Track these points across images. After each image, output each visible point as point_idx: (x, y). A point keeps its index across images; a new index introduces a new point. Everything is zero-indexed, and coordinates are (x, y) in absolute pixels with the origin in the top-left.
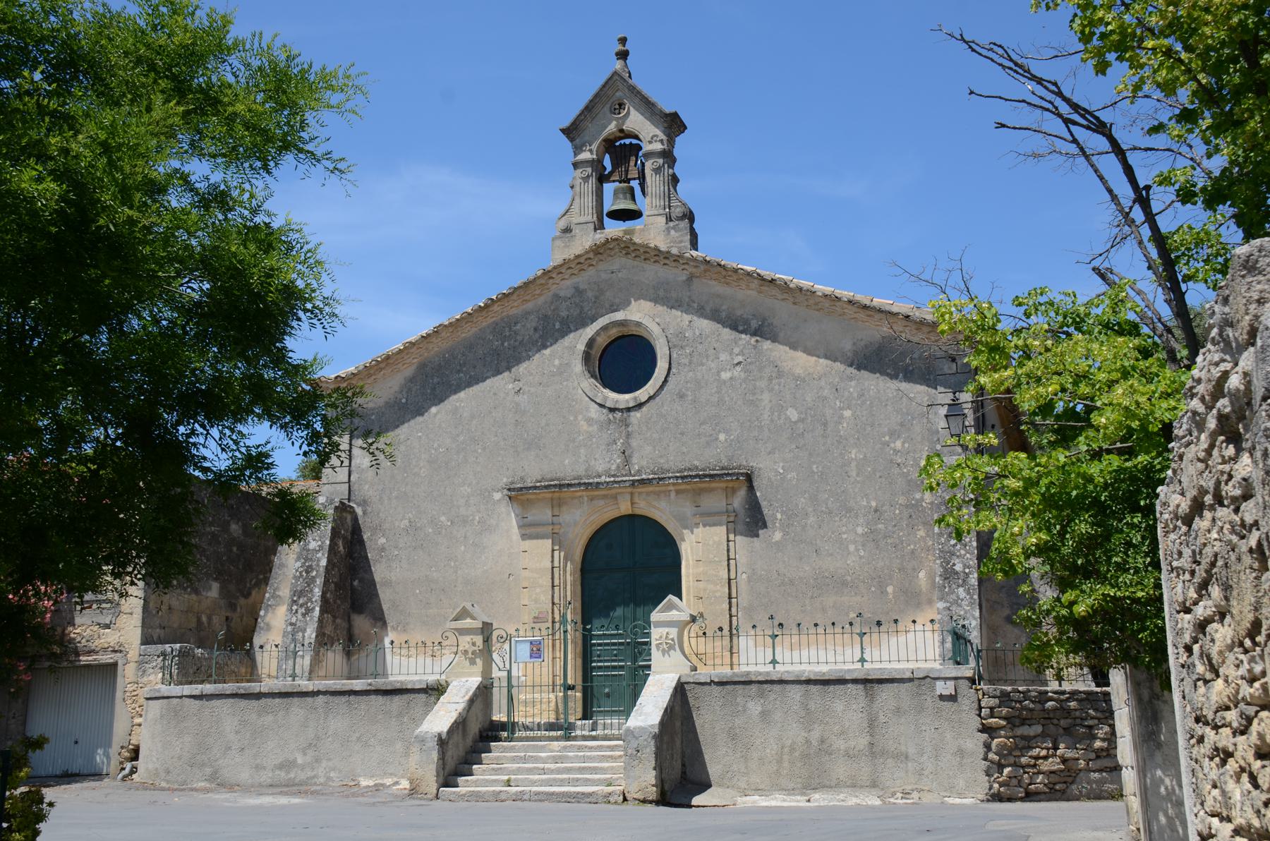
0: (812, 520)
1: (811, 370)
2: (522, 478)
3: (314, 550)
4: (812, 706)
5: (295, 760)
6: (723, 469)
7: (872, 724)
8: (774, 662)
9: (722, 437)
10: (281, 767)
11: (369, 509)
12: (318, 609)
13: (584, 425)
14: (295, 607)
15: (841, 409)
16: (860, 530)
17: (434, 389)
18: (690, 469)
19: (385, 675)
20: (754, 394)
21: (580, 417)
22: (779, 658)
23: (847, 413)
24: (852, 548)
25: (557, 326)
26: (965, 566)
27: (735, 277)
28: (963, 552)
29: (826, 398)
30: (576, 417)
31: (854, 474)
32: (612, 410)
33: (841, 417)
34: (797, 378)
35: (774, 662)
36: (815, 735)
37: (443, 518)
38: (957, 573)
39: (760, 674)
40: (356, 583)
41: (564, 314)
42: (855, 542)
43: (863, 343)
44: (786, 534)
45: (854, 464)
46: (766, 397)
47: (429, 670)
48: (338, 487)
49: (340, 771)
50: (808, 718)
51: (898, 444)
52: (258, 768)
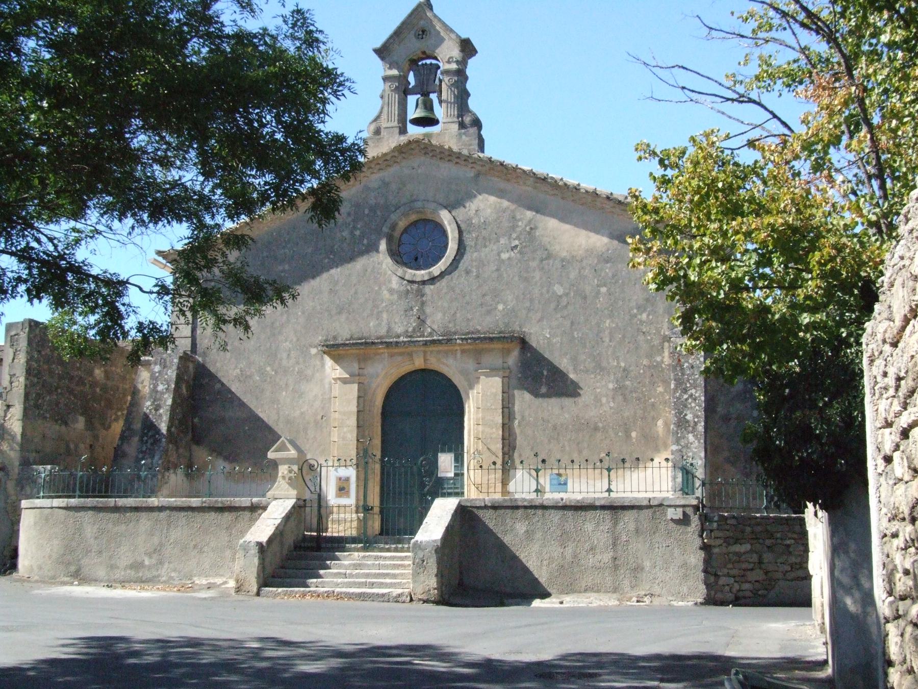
16: (611, 386)
25: (366, 212)
28: (693, 405)
32: (411, 282)
35: (609, 490)
38: (688, 421)
40: (196, 420)
41: (372, 202)
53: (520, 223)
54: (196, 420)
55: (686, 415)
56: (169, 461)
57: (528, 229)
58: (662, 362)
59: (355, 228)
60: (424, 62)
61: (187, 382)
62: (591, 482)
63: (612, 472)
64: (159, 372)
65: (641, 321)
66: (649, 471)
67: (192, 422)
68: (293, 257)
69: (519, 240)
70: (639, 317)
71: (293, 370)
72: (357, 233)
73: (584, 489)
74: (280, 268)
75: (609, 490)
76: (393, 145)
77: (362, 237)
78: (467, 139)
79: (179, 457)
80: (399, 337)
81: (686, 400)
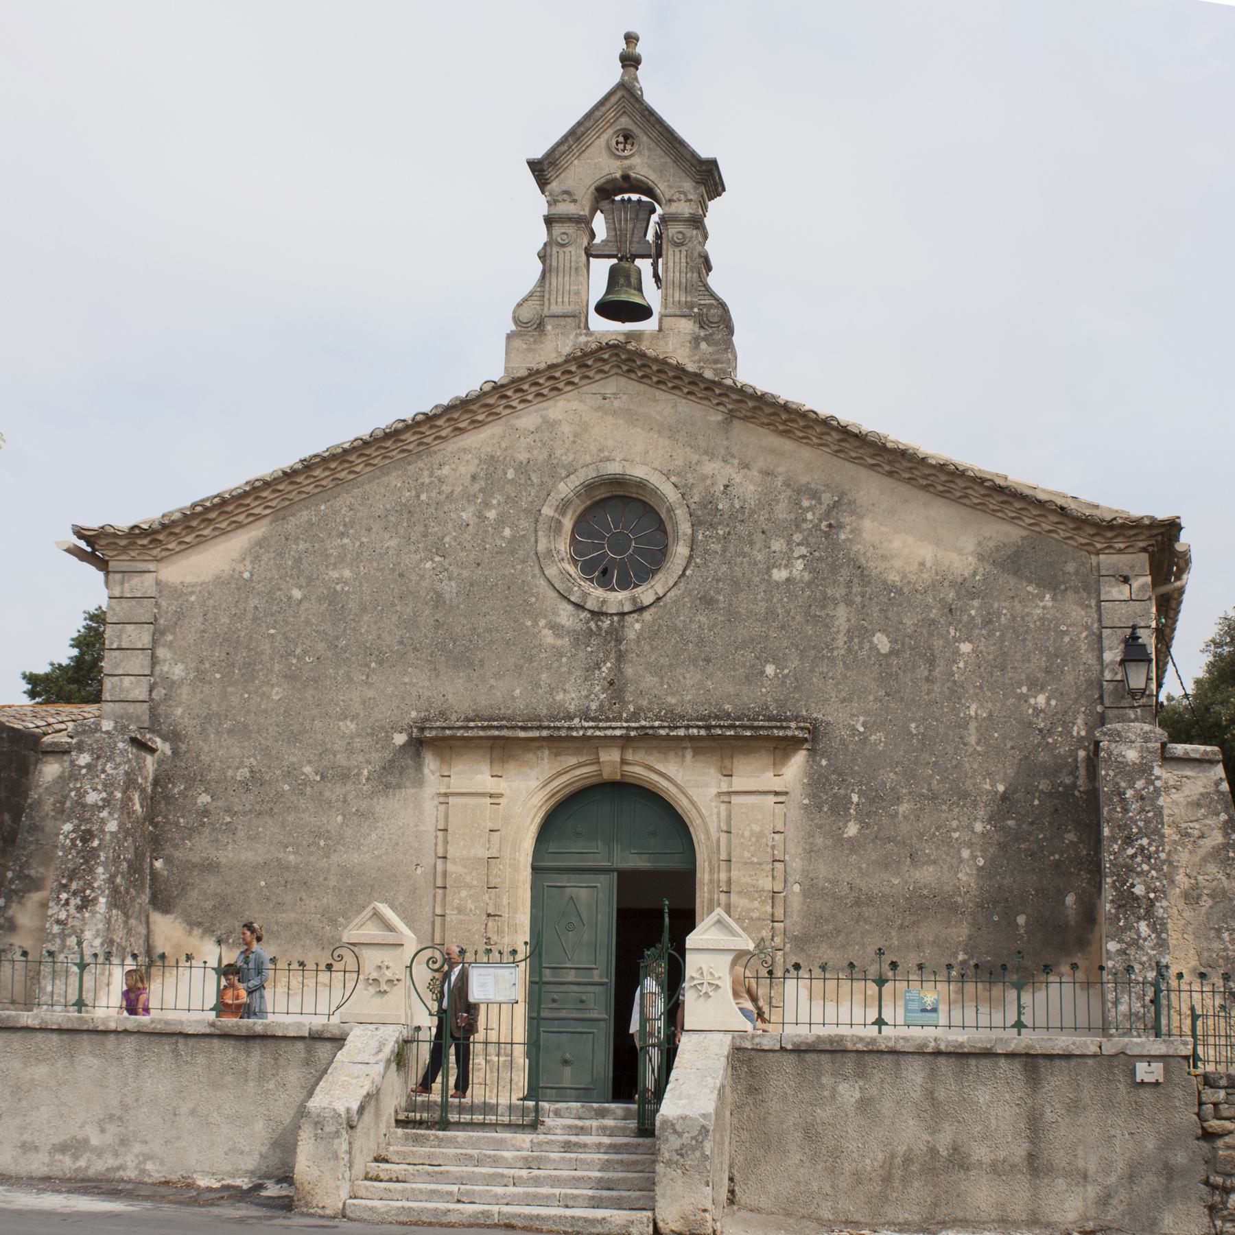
0: (904, 808)
1: (913, 578)
2: (442, 714)
3: (95, 806)
4: (941, 1094)
5: (86, 1141)
6: (769, 719)
7: (1034, 1126)
8: (880, 1022)
9: (770, 670)
10: (63, 1148)
11: (183, 747)
12: (102, 900)
13: (548, 638)
14: (64, 896)
15: (956, 640)
16: (978, 827)
17: (298, 560)
18: (717, 717)
19: (262, 1013)
20: (823, 607)
21: (542, 623)
22: (887, 1016)
23: (966, 647)
24: (965, 853)
25: (511, 474)
26: (1149, 889)
27: (802, 423)
28: (1145, 867)
29: (933, 622)
30: (536, 624)
31: (972, 740)
32: (597, 615)
33: (956, 652)
34: (888, 587)
35: (880, 1022)
36: (944, 1141)
37: (308, 769)
38: (1137, 898)
39: (861, 1039)
40: (158, 864)
41: (523, 456)
42: (970, 845)
43: (992, 544)
44: (864, 826)
45: (972, 726)
46: (842, 612)
47: (309, 1008)
48: (131, 708)
49: (162, 1163)
50: (934, 1110)
51: (1041, 700)
52: (27, 1148)
53: (809, 516)
54: (158, 864)
55: (1133, 886)
56: (112, 942)
57: (824, 525)
58: (1075, 786)
59: (487, 505)
60: (626, 196)
61: (143, 790)
62: (984, 1009)
63: (888, 987)
64: (88, 766)
65: (1035, 709)
66: (1054, 989)
67: (152, 865)
68: (359, 554)
69: (808, 545)
70: (1032, 701)
71: (358, 775)
72: (492, 514)
73: (983, 1020)
74: (335, 574)
75: (80, 1004)
76: (566, 350)
77: (501, 521)
78: (711, 350)
79: (129, 932)
80: (571, 719)
81: (1133, 856)
